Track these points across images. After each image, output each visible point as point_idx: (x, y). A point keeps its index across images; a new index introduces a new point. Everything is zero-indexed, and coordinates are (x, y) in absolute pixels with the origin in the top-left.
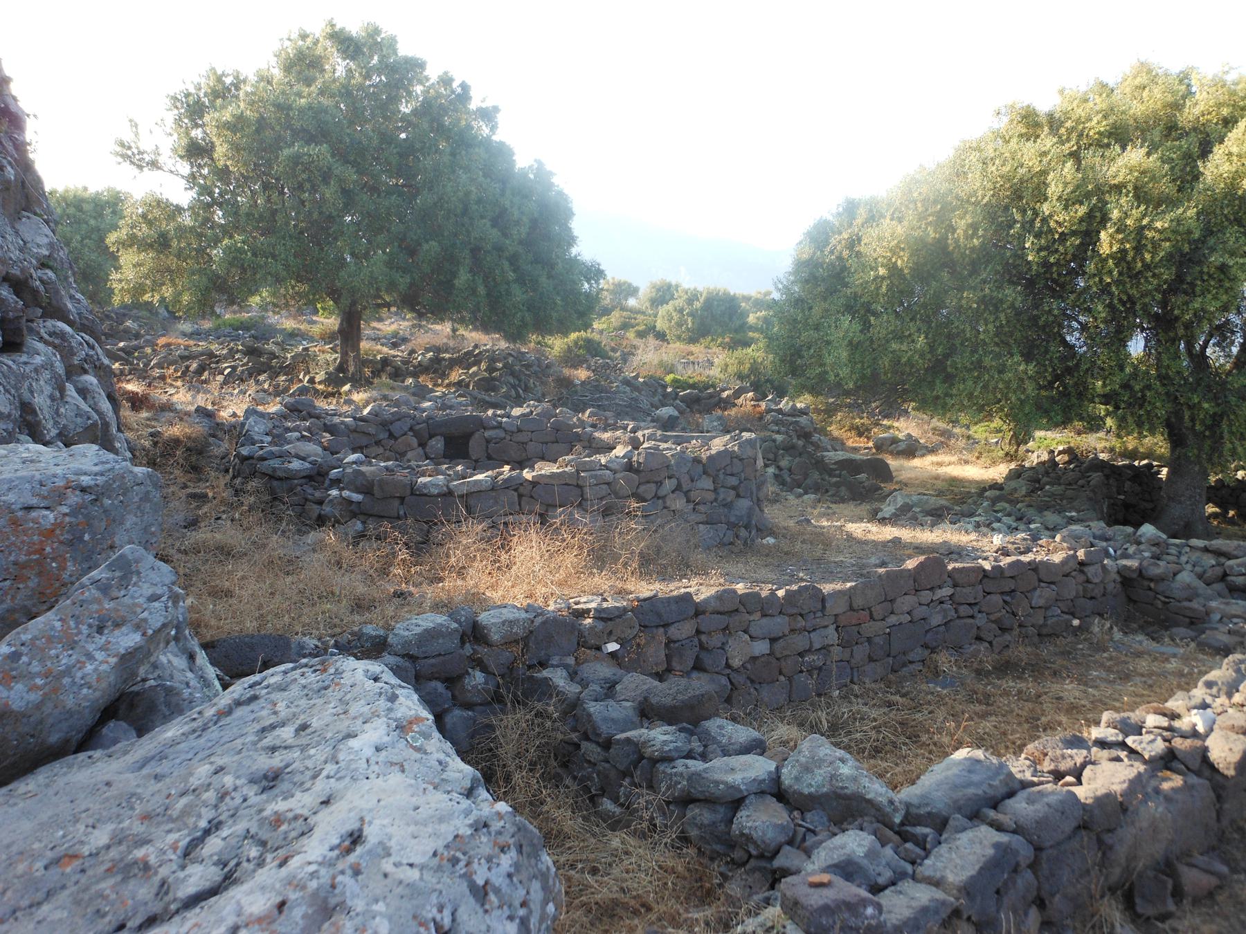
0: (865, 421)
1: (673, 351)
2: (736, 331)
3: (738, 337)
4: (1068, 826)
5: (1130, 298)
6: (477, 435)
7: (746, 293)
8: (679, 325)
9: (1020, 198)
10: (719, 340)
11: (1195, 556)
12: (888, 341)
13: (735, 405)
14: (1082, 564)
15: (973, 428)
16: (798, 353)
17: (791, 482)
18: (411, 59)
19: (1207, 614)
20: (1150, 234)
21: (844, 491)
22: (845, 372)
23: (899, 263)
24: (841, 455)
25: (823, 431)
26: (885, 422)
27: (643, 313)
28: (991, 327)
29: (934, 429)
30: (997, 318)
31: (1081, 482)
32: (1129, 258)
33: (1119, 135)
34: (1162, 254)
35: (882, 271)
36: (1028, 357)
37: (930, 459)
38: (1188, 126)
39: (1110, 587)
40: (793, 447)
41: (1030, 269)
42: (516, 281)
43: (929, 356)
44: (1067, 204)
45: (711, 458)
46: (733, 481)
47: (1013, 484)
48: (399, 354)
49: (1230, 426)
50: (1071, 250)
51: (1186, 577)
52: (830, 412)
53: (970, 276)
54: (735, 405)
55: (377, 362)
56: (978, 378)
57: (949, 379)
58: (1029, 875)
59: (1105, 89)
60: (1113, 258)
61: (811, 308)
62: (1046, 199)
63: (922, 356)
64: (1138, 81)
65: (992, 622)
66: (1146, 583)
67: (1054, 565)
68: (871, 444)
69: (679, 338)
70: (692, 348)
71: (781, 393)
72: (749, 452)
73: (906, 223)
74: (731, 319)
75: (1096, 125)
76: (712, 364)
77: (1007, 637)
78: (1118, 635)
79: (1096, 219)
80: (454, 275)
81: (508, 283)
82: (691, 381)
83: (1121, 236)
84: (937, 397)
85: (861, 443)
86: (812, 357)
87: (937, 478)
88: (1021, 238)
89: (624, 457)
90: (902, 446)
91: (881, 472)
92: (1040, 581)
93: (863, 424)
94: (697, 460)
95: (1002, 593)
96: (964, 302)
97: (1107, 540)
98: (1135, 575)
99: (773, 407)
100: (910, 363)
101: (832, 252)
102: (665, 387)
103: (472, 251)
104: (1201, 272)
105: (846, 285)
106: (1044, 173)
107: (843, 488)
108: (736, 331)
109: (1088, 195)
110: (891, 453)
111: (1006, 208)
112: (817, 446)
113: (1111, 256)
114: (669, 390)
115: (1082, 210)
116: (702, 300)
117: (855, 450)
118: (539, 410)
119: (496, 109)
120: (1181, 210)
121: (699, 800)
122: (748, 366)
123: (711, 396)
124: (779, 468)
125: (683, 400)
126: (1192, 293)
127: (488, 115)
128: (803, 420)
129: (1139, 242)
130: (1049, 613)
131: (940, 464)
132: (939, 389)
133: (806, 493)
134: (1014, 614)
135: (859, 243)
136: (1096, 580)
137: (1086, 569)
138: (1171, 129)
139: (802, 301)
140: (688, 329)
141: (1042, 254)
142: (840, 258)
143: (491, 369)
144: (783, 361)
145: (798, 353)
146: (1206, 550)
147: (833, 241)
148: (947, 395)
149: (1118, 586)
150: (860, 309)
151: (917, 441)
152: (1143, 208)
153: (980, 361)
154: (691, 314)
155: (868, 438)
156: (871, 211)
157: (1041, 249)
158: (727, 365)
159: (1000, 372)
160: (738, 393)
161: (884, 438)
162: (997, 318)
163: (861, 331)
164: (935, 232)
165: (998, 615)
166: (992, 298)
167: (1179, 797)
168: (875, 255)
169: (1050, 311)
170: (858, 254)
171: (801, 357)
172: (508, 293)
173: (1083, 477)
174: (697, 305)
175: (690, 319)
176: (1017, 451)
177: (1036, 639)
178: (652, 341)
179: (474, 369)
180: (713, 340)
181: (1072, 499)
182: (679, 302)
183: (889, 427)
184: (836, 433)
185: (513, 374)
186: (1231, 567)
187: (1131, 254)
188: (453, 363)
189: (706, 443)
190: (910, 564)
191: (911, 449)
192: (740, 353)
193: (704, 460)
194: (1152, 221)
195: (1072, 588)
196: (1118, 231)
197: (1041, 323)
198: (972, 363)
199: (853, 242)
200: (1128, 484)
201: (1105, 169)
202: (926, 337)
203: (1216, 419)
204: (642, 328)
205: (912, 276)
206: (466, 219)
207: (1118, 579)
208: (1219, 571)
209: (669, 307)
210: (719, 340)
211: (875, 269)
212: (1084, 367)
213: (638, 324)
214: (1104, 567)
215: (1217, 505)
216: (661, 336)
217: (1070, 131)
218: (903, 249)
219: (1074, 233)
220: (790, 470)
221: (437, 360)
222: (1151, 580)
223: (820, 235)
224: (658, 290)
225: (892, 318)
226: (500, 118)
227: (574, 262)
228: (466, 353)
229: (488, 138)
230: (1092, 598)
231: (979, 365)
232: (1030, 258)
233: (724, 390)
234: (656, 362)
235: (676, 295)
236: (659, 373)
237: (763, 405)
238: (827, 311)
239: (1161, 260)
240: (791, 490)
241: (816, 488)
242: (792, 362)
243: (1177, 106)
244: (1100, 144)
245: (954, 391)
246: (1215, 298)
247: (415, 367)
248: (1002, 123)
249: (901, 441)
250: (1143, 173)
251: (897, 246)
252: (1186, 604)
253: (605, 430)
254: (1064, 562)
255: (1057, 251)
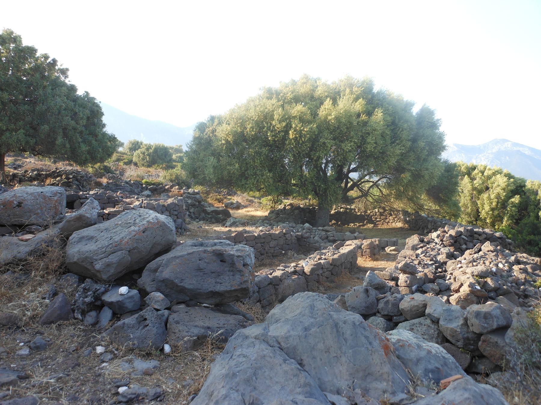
0: (221, 197)
1: (141, 171)
2: (168, 162)
3: (169, 164)
4: (267, 283)
5: (299, 152)
6: (77, 202)
7: (171, 146)
8: (143, 159)
9: (267, 119)
10: (161, 166)
11: (319, 232)
12: (226, 166)
13: (171, 191)
14: (285, 234)
15: (262, 199)
16: (195, 170)
17: (195, 217)
18: (30, 47)
19: (320, 247)
20: (303, 132)
21: (213, 220)
22: (212, 176)
23: (229, 139)
24: (212, 209)
25: (205, 201)
26: (229, 197)
27: (126, 154)
28: (259, 161)
29: (247, 200)
30: (260, 158)
31: (292, 214)
32: (298, 140)
33: (297, 100)
34: (307, 139)
35: (223, 142)
36: (270, 171)
37: (245, 210)
38: (317, 97)
39: (294, 241)
40: (195, 205)
41: (270, 142)
42: (82, 142)
43: (239, 171)
44: (280, 122)
45: (168, 205)
46: (176, 213)
47: (271, 215)
48: (20, 172)
49: (329, 192)
50: (282, 137)
51: (316, 238)
52: (208, 193)
53: (252, 144)
54: (171, 191)
55: (11, 176)
56: (255, 178)
57: (246, 178)
58: (257, 294)
59: (294, 83)
60: (294, 139)
61: (199, 154)
62: (274, 120)
63: (237, 171)
64: (303, 81)
65: (259, 252)
66: (303, 239)
67: (276, 234)
68: (223, 205)
69: (143, 165)
70: (149, 169)
71: (189, 187)
72: (181, 203)
73: (231, 126)
74: (165, 157)
75: (290, 96)
76: (159, 176)
77: (263, 257)
78: (295, 255)
79: (288, 127)
80: (55, 139)
81: (79, 143)
82: (153, 182)
83: (295, 133)
84: (243, 185)
85: (220, 205)
86: (200, 171)
87: (247, 216)
88: (267, 132)
89: (139, 205)
90: (235, 206)
91: (228, 215)
92: (272, 239)
93: (220, 198)
94: (164, 206)
95: (261, 243)
96: (250, 153)
97: (293, 228)
98: (300, 237)
99: (186, 192)
100: (234, 173)
101: (206, 134)
102: (142, 185)
103: (63, 129)
104: (318, 144)
105: (211, 146)
106: (273, 111)
107: (213, 219)
108: (168, 162)
109: (286, 119)
110: (231, 208)
111: (262, 122)
112: (203, 206)
113: (293, 139)
114: (144, 186)
115: (284, 124)
116: (153, 149)
117: (218, 207)
118: (101, 191)
119: (67, 70)
120: (312, 125)
121: (168, 316)
122: (174, 176)
123: (161, 188)
124: (190, 212)
125: (150, 190)
126: (316, 151)
127: (64, 72)
128: (198, 196)
129: (301, 134)
130: (275, 249)
131: (248, 211)
132: (243, 182)
133: (200, 221)
134: (265, 249)
135: (216, 132)
136: (289, 239)
137: (286, 235)
138: (312, 98)
139: (196, 151)
140: (147, 161)
141: (273, 137)
142: (209, 136)
143: (68, 178)
144: (190, 173)
145: (195, 170)
146: (323, 230)
147: (207, 131)
148: (246, 184)
149: (296, 241)
150: (217, 155)
151: (240, 203)
152: (301, 124)
153: (256, 173)
154: (148, 155)
155: (223, 203)
156: (219, 120)
157: (272, 136)
158: (165, 176)
159: (262, 176)
160: (172, 187)
161: (228, 203)
162: (260, 158)
163: (217, 162)
164: (240, 129)
165: (260, 250)
166: (259, 151)
167: (296, 280)
168: (221, 136)
169: (276, 156)
170: (215, 136)
171: (197, 172)
172: (80, 147)
173: (293, 212)
174: (151, 151)
175: (148, 157)
176: (275, 206)
177: (272, 257)
178: (133, 167)
179: (59, 178)
180: (158, 166)
181: (288, 219)
182: (143, 150)
183: (230, 199)
184: (210, 202)
185: (77, 180)
186: (329, 234)
187: (299, 138)
188: (47, 176)
189: (165, 200)
190: (233, 235)
191: (238, 207)
192: (170, 171)
193: (166, 206)
194: (304, 128)
195: (282, 241)
196: (295, 131)
197: (274, 160)
198: (253, 173)
199: (214, 131)
200: (307, 214)
201: (291, 111)
202: (239, 164)
203: (326, 190)
204: (126, 161)
205: (233, 144)
206: (60, 117)
207: (296, 239)
208: (325, 236)
209: (139, 151)
210: (161, 166)
211: (221, 141)
212: (287, 174)
213: (124, 159)
214: (291, 235)
215: (335, 220)
216: (136, 164)
217: (282, 97)
218: (230, 135)
219: (282, 131)
220: (194, 213)
221: (39, 175)
222: (305, 238)
223: (201, 127)
224: (133, 144)
225: (227, 158)
226: (69, 73)
227: (105, 134)
228: (53, 172)
229: (64, 82)
230: (288, 245)
231: (255, 174)
232: (270, 139)
233: (166, 186)
234: (136, 175)
235: (141, 146)
236: (139, 179)
237: (182, 191)
238: (205, 155)
239: (307, 140)
240: (195, 220)
241: (203, 219)
242: (193, 173)
243: (314, 91)
244: (290, 103)
245: (248, 183)
246: (322, 152)
247: (28, 178)
248: (261, 93)
249: (234, 203)
250: (302, 113)
251: (228, 133)
252: (314, 244)
253: (126, 198)
254: (279, 233)
255: (277, 137)
